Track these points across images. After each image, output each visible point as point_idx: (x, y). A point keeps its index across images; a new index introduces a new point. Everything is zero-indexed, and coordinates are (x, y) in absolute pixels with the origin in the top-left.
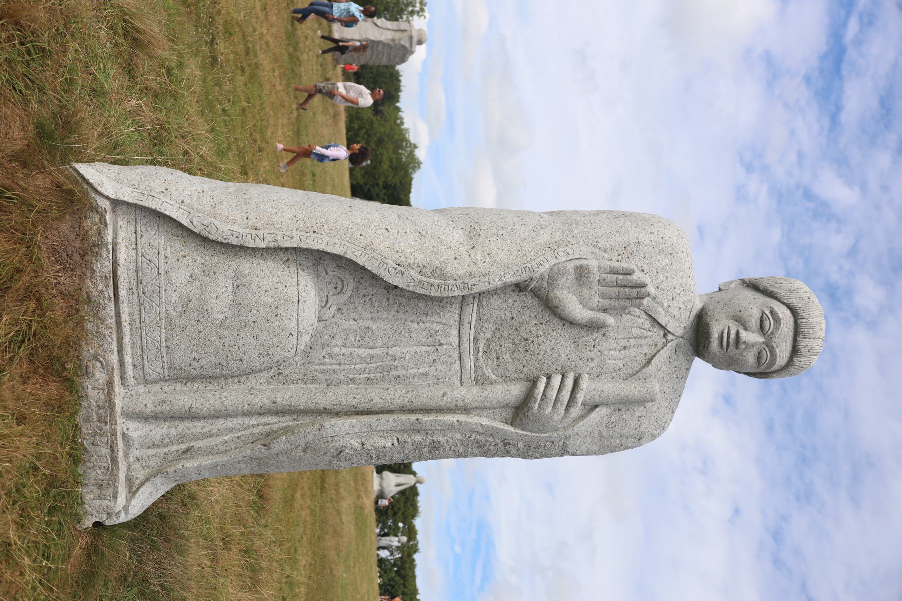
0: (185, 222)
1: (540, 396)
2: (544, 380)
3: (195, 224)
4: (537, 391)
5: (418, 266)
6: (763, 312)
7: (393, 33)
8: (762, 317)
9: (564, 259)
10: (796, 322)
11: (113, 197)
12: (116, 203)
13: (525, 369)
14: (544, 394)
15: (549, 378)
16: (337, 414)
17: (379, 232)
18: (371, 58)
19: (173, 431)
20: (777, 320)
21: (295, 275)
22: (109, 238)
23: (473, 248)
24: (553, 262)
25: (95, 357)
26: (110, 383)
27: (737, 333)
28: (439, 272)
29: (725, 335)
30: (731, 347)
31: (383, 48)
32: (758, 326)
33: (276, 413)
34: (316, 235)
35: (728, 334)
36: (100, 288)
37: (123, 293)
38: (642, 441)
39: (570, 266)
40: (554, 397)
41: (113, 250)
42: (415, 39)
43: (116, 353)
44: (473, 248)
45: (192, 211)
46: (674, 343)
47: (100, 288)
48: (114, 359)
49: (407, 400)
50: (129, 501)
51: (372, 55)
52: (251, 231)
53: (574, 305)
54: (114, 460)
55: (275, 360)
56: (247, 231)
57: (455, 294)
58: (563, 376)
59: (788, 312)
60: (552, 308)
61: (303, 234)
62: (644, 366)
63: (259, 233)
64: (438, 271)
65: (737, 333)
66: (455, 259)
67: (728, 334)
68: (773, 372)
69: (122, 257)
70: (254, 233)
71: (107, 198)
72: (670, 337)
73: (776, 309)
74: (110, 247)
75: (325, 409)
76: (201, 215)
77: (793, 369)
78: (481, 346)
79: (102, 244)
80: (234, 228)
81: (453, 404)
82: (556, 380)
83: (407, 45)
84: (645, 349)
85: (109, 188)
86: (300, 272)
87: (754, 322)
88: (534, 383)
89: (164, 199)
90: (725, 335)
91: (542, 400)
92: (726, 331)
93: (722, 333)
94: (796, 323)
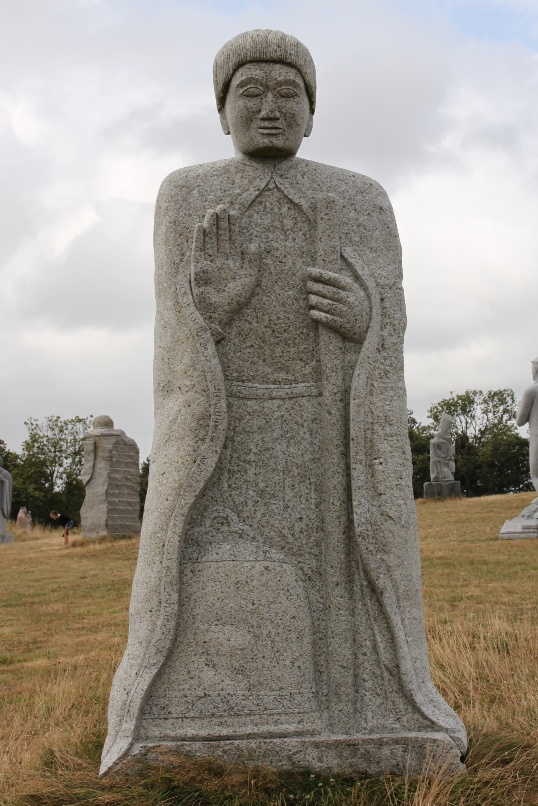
0: (154, 671)
1: (328, 316)
2: (316, 314)
3: (155, 661)
4: (324, 319)
5: (196, 442)
6: (242, 94)
7: (99, 459)
8: (247, 96)
9: (191, 297)
10: (251, 62)
11: (130, 740)
12: (137, 738)
13: (305, 331)
14: (327, 312)
15: (312, 307)
16: (350, 521)
17: (165, 481)
18: (132, 488)
19: (369, 684)
20: (249, 81)
21: (206, 564)
22: (171, 744)
23: (180, 388)
24: (192, 308)
25: (289, 758)
26: (316, 745)
27: (263, 119)
28: (203, 420)
29: (265, 131)
30: (276, 124)
31: (117, 472)
32: (254, 99)
33: (351, 582)
34: (166, 544)
35: (264, 128)
36: (220, 753)
37: (225, 732)
38: (385, 207)
39: (196, 291)
40: (331, 302)
41: (184, 740)
42: (105, 431)
43: (285, 739)
44: (180, 388)
45: (144, 665)
46: (278, 180)
47: (220, 753)
48: (293, 741)
49: (335, 451)
50: (440, 729)
51: (128, 487)
52: (162, 607)
53: (236, 287)
54: (396, 742)
55: (295, 583)
56: (162, 612)
57: (224, 405)
58: (311, 293)
59: (241, 71)
60: (239, 309)
61: (165, 556)
62: (301, 210)
63: (164, 599)
64: (201, 422)
65: (263, 119)
66: (189, 406)
67: (264, 128)
68: (304, 81)
69: (191, 732)
70: (164, 604)
71: (132, 745)
72: (271, 186)
73: (238, 82)
74: (180, 743)
75: (344, 533)
76: (147, 656)
77: (300, 62)
78: (282, 375)
79: (177, 752)
80: (159, 623)
81: (340, 405)
82: (314, 299)
83: (113, 440)
84: (285, 209)
85: (123, 744)
86: (204, 559)
87: (252, 104)
88: (317, 322)
89: (133, 692)
90: (265, 131)
91: (332, 314)
92: (261, 130)
93: (263, 134)
94: (253, 61)
